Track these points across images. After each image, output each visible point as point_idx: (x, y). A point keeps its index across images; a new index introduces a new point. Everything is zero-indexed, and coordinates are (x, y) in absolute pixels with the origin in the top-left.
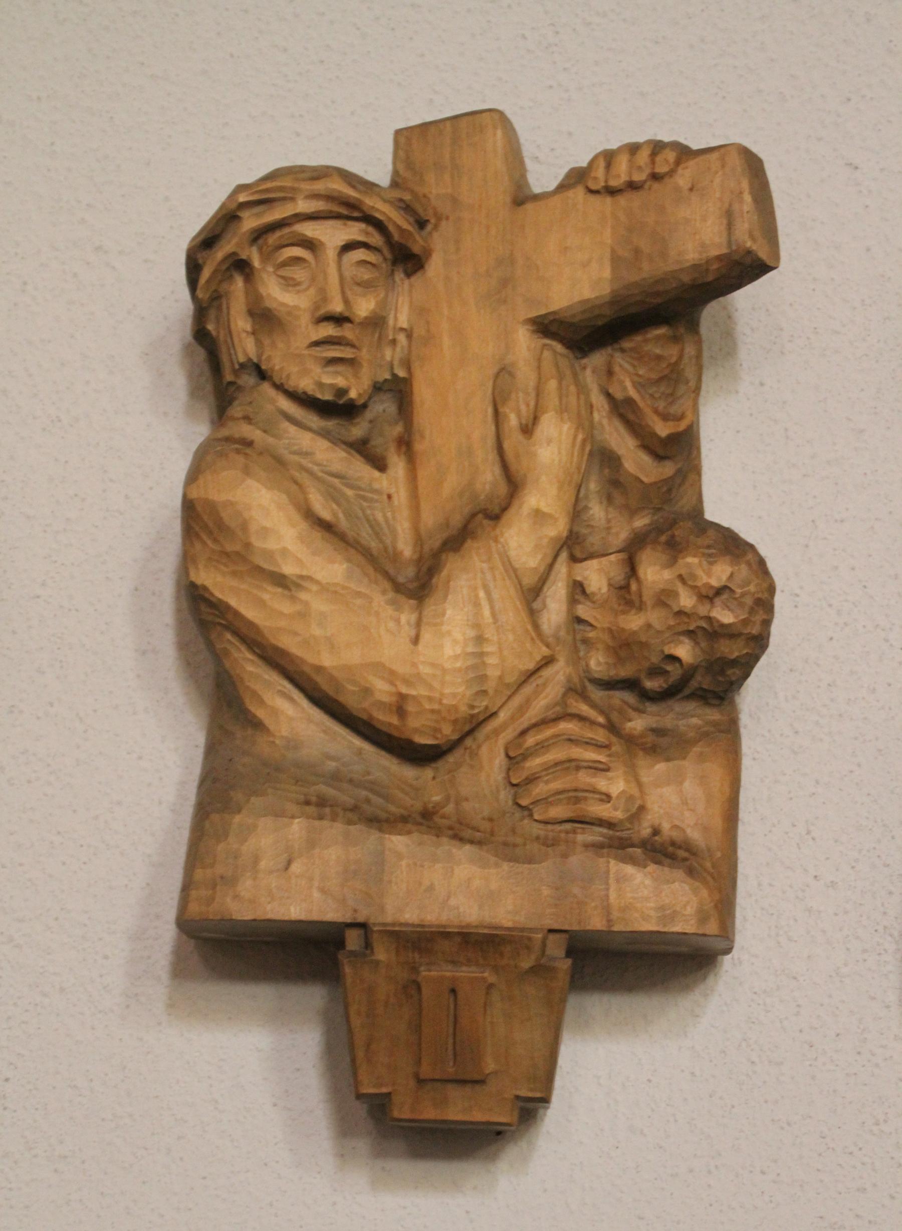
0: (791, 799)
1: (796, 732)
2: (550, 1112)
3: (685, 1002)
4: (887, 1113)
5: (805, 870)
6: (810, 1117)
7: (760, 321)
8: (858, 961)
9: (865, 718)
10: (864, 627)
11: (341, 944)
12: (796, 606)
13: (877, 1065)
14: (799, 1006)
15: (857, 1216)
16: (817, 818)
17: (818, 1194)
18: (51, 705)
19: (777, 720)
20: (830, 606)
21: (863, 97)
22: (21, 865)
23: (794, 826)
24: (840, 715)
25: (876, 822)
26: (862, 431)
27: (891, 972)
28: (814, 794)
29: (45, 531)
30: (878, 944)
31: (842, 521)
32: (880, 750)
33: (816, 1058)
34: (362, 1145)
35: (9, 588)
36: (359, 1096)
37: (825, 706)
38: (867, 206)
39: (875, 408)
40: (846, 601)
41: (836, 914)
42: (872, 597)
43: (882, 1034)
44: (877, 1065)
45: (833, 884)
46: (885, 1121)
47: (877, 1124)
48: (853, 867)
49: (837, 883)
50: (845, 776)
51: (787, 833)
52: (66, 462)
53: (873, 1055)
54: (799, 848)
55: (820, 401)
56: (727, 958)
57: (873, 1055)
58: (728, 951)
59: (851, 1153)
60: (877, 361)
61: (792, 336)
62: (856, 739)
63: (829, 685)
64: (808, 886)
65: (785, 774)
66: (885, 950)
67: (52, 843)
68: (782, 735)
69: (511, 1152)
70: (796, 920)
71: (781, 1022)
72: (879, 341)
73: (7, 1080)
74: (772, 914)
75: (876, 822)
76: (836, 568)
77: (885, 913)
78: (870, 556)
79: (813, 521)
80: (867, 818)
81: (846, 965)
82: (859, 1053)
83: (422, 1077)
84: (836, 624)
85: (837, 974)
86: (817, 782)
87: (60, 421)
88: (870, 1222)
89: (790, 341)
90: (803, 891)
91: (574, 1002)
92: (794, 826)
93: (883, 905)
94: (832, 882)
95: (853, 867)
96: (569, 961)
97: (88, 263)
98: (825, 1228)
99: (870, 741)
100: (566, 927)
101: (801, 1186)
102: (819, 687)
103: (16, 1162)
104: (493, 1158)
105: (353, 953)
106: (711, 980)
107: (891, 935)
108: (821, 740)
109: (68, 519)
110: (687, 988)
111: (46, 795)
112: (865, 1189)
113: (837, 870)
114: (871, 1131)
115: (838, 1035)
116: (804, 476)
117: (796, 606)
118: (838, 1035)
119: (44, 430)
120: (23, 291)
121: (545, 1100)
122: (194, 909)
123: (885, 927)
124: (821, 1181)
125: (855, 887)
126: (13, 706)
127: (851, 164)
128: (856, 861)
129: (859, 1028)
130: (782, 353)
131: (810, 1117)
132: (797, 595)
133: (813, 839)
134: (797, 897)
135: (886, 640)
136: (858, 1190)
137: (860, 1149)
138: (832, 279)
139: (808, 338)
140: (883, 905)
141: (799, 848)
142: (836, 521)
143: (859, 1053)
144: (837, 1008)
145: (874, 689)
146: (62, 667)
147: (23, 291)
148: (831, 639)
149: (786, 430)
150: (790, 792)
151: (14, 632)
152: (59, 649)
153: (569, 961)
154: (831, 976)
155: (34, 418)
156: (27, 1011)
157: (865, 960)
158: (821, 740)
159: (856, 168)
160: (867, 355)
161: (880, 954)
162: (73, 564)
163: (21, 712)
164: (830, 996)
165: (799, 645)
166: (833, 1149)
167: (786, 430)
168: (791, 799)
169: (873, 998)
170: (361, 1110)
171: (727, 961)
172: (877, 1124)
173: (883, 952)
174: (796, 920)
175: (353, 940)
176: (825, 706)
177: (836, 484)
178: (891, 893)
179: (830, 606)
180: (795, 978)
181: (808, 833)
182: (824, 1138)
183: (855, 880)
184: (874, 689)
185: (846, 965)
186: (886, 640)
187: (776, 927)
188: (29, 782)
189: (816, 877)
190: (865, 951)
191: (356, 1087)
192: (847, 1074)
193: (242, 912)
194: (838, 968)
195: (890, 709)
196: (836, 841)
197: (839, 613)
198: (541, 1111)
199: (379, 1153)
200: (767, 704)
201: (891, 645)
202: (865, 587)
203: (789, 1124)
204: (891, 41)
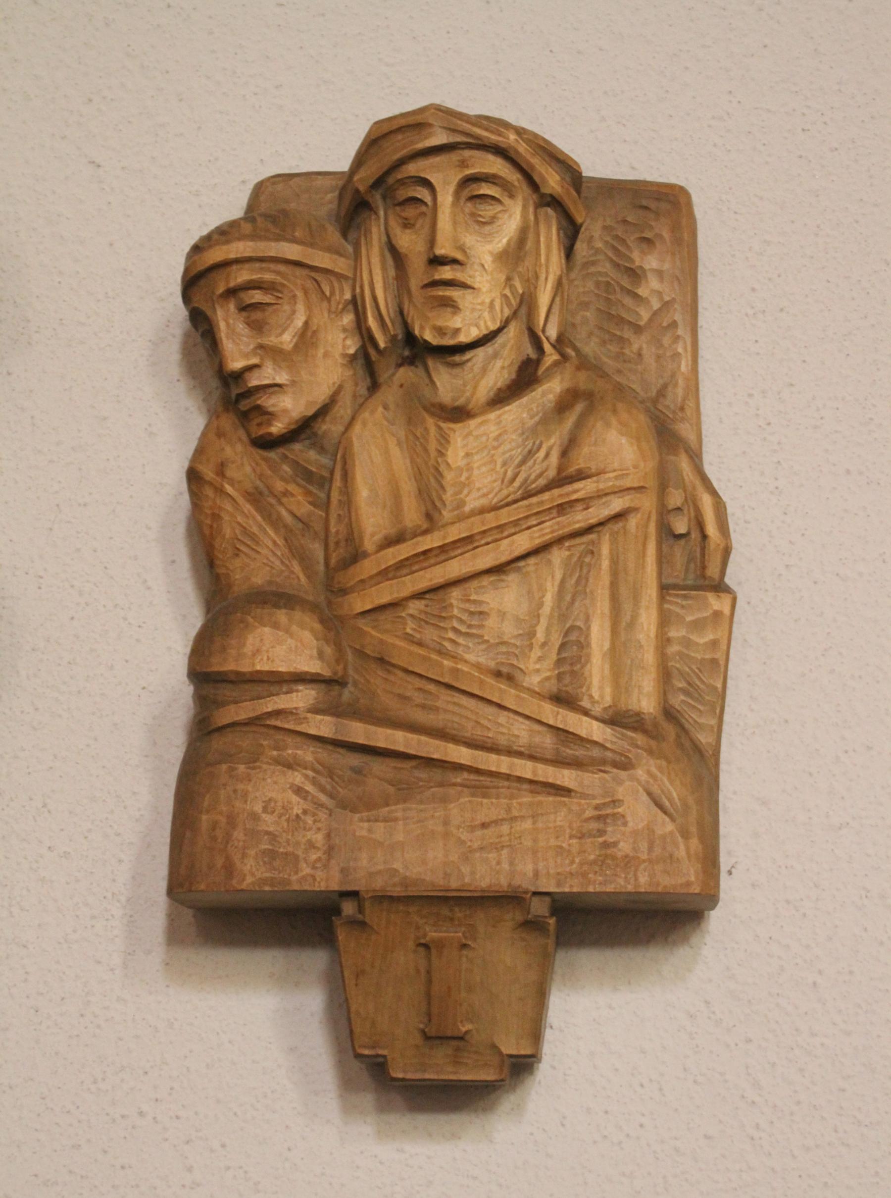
0: (29, 773)
1: (37, 709)
3: (682, 953)
4: (105, 1072)
5: (40, 842)
6: (32, 1079)
7: (8, 313)
8: (86, 927)
9: (103, 694)
10: (104, 606)
12: (40, 588)
13: (99, 1027)
14: (26, 973)
15: (70, 1172)
16: (53, 791)
17: (34, 1153)
19: (18, 698)
20: (72, 586)
21: (104, 98)
23: (31, 799)
24: (79, 692)
25: (109, 793)
26: (105, 419)
27: (117, 936)
28: (51, 768)
30: (106, 910)
31: (85, 505)
32: (115, 725)
33: (41, 1022)
36: (358, 1056)
37: (64, 683)
38: (109, 203)
39: (118, 396)
40: (88, 581)
41: (68, 883)
42: (112, 577)
43: (105, 996)
44: (99, 1027)
45: (66, 855)
46: (104, 1080)
47: (95, 1082)
48: (86, 837)
49: (69, 853)
50: (82, 749)
51: (24, 807)
53: (95, 1016)
54: (35, 821)
55: (65, 390)
57: (95, 1016)
59: (68, 1112)
60: (120, 352)
61: (39, 327)
62: (93, 714)
63: (69, 663)
64: (41, 857)
65: (24, 750)
66: (113, 916)
68: (22, 712)
70: (28, 891)
71: (9, 989)
72: (121, 333)
74: (6, 885)
75: (109, 793)
76: (78, 550)
77: (114, 880)
78: (111, 538)
79: (58, 505)
80: (101, 790)
81: (75, 931)
82: (82, 1015)
83: (429, 1034)
84: (78, 604)
85: (66, 940)
86: (55, 756)
88: (82, 1177)
89: (37, 332)
90: (37, 862)
91: (563, 959)
92: (31, 799)
93: (112, 872)
94: (65, 852)
95: (86, 837)
96: (554, 918)
98: (39, 1185)
99: (107, 715)
101: (18, 1147)
102: (59, 665)
104: (489, 1109)
107: (118, 901)
108: (60, 716)
112: (80, 1146)
113: (71, 840)
114: (89, 1089)
115: (63, 999)
116: (50, 461)
117: (40, 588)
118: (63, 999)
123: (113, 894)
124: (39, 1140)
125: (87, 857)
127: (93, 162)
128: (90, 831)
129: (83, 991)
130: (29, 343)
131: (32, 1079)
132: (41, 577)
133: (49, 812)
134: (31, 868)
135: (125, 619)
136: (73, 1146)
137: (78, 1107)
138: (78, 273)
139: (54, 329)
140: (112, 872)
141: (35, 821)
142: (80, 505)
143: (82, 1015)
144: (64, 973)
145: (112, 666)
148: (72, 618)
149: (32, 417)
150: (28, 767)
153: (554, 918)
154: (60, 943)
157: (93, 926)
158: (60, 716)
159: (99, 166)
160: (110, 346)
161: (107, 920)
164: (58, 962)
165: (42, 625)
166: (52, 1109)
167: (32, 417)
168: (29, 773)
169: (99, 962)
172: (95, 1082)
173: (111, 918)
174: (28, 891)
176: (64, 683)
177: (80, 469)
178: (120, 861)
179: (72, 586)
180: (25, 946)
181: (45, 806)
182: (44, 1099)
183: (88, 850)
184: (112, 666)
185: (75, 931)
186: (125, 619)
187: (9, 898)
189: (49, 848)
190: (93, 917)
192: (70, 1037)
194: (67, 935)
195: (127, 684)
196: (71, 813)
197: (81, 593)
198: (535, 1065)
200: (10, 683)
201: (129, 623)
202: (106, 568)
203: (11, 1088)
204: (129, 46)
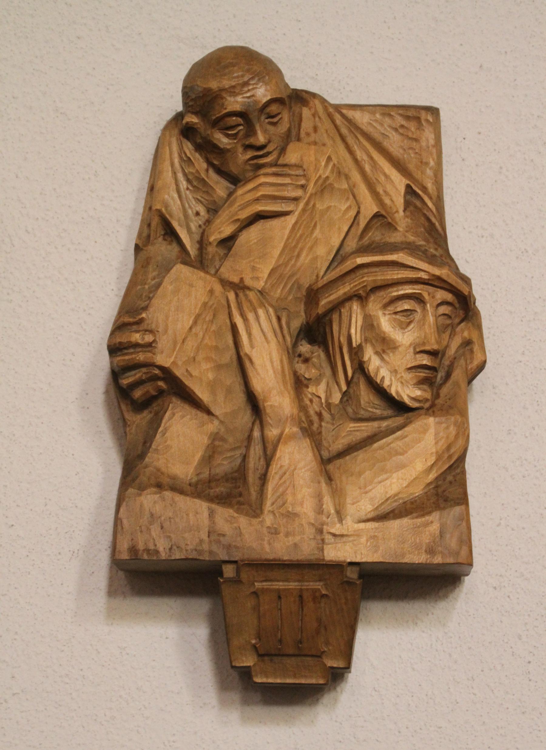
2: (350, 675)
11: (221, 574)
18: (534, 428)
22: (523, 528)
29: (522, 321)
34: (235, 696)
35: (502, 356)
36: (233, 667)
52: (532, 277)
56: (466, 578)
58: (467, 575)
67: (542, 514)
69: (327, 699)
73: (529, 662)
87: (527, 252)
97: (540, 153)
100: (358, 560)
103: (541, 714)
105: (229, 581)
106: (457, 590)
109: (536, 313)
110: (446, 596)
111: (535, 485)
119: (517, 258)
120: (500, 173)
121: (348, 667)
122: (457, 510)
126: (510, 430)
146: (538, 405)
147: (500, 173)
151: (507, 384)
152: (536, 393)
155: (511, 251)
156: (537, 619)
162: (540, 341)
163: (515, 433)
170: (235, 674)
171: (467, 580)
175: (229, 571)
188: (524, 477)
191: (231, 662)
193: (122, 558)
198: (346, 675)
199: (246, 702)
